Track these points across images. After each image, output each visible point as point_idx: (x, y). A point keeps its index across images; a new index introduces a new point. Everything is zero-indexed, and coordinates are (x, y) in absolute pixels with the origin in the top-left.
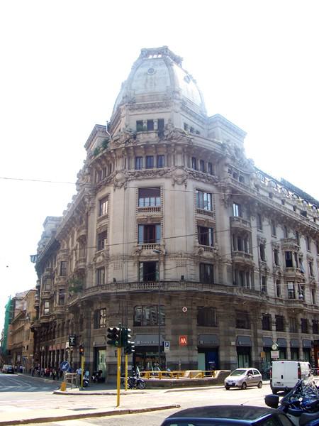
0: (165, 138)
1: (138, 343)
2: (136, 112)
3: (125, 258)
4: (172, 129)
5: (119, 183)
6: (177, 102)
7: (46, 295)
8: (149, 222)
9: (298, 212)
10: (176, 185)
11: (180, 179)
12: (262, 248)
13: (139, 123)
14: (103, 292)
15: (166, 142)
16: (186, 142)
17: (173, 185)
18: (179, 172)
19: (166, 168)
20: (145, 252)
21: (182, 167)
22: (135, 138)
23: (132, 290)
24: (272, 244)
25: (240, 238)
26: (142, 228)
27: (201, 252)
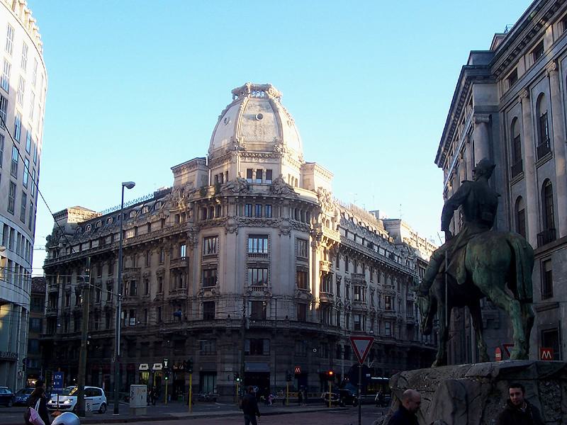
1: (322, 370)
3: (236, 297)
12: (338, 284)
14: (216, 325)
19: (273, 219)
21: (287, 220)
27: (299, 294)
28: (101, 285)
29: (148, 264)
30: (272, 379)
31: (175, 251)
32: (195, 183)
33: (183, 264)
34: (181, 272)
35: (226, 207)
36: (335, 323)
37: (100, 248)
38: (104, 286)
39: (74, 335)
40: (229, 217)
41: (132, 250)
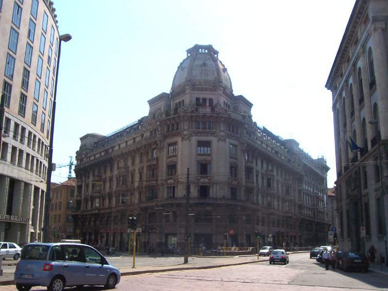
0: (215, 113)
2: (196, 92)
4: (220, 108)
5: (186, 137)
6: (222, 88)
7: (97, 194)
8: (204, 163)
9: (273, 151)
10: (220, 142)
11: (222, 138)
12: (257, 176)
13: (198, 99)
15: (215, 115)
16: (227, 116)
17: (218, 141)
18: (222, 134)
19: (214, 130)
20: (202, 180)
21: (224, 131)
22: (197, 110)
23: (195, 202)
24: (262, 174)
25: (249, 171)
26: (199, 165)
27: (232, 181)
28: (106, 179)
29: (133, 164)
30: (214, 238)
31: (150, 154)
32: (162, 109)
33: (154, 162)
34: (153, 169)
35: (182, 123)
36: (255, 201)
37: (105, 155)
38: (108, 179)
39: (90, 211)
40: (184, 130)
41: (124, 156)
